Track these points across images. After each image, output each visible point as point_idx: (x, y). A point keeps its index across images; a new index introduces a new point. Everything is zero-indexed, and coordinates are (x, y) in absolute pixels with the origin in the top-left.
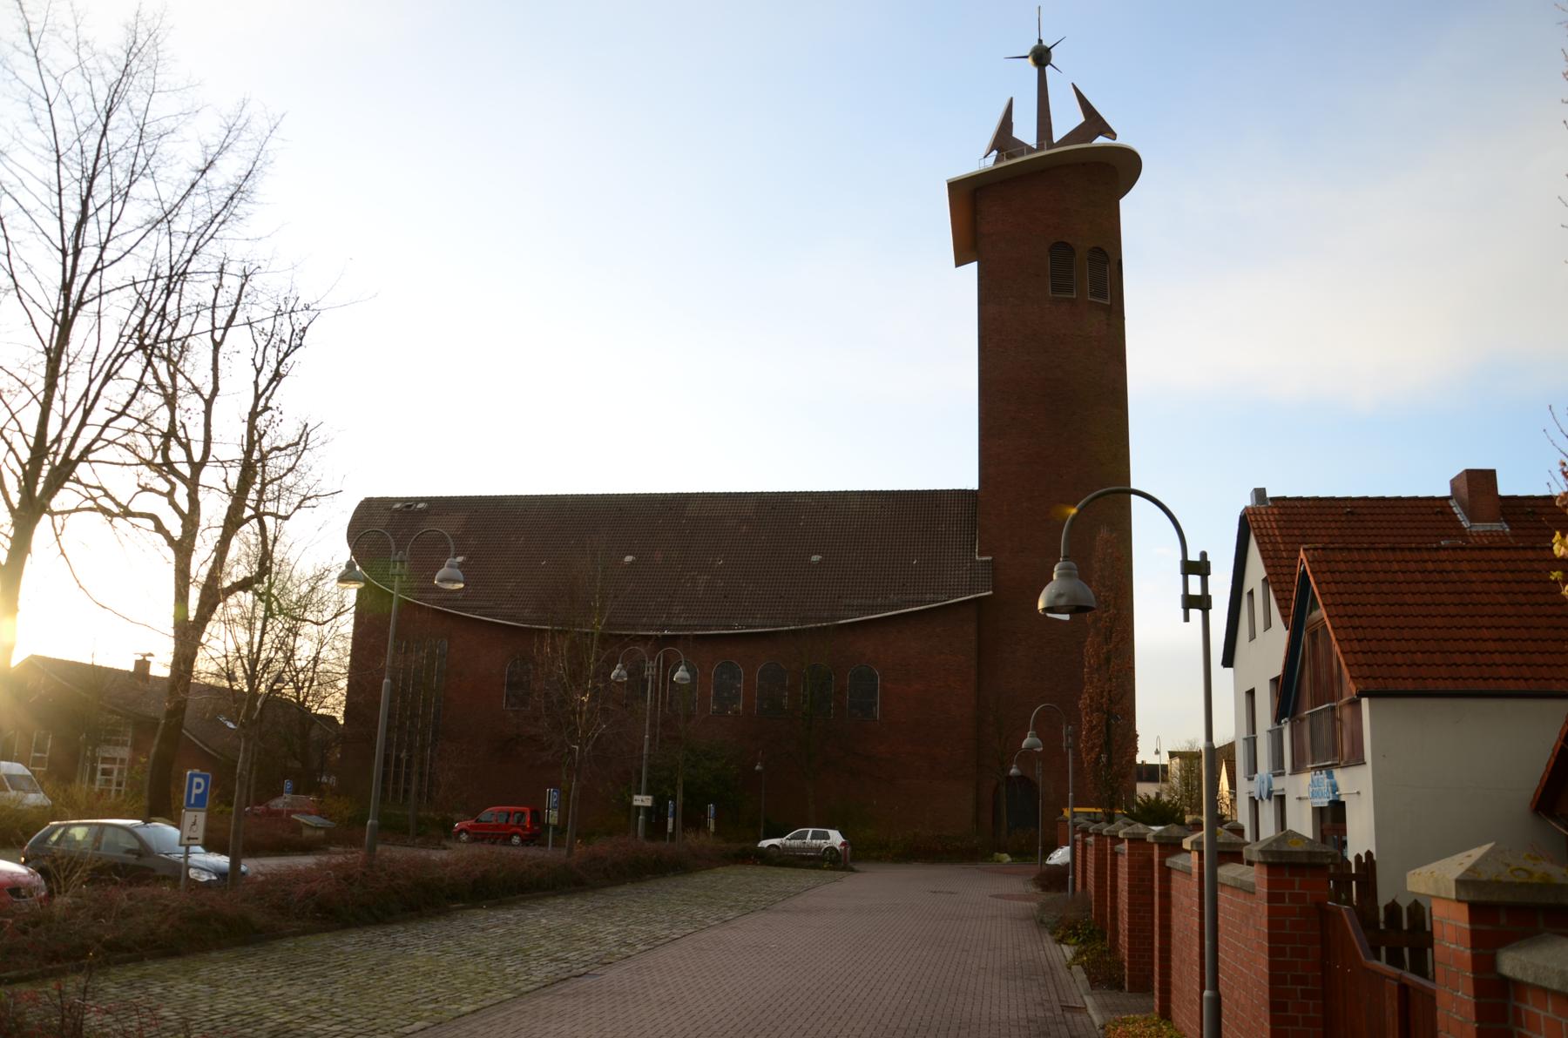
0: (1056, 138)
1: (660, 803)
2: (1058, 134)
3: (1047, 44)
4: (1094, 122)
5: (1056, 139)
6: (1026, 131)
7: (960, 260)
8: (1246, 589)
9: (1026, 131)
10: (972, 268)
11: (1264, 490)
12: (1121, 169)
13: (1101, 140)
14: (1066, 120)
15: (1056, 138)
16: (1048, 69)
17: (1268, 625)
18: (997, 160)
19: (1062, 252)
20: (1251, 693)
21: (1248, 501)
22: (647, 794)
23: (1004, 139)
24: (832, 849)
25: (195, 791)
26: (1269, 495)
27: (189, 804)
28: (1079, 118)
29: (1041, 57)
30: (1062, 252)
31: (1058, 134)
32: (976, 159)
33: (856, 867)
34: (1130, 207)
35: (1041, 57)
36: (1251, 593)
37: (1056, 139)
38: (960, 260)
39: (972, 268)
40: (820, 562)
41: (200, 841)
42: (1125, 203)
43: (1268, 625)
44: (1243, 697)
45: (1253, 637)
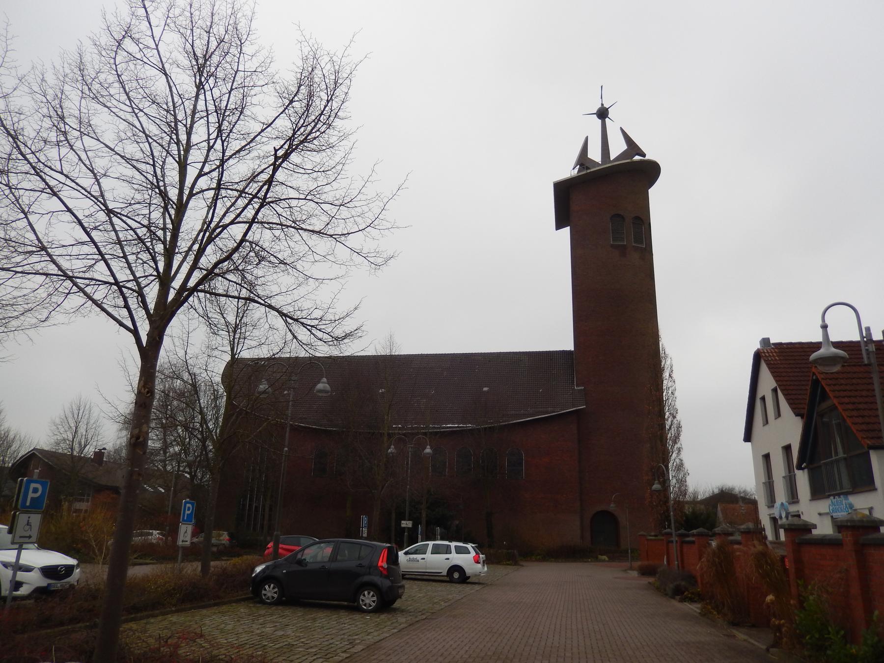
0: (612, 157)
1: (415, 526)
2: (613, 155)
3: (606, 106)
4: (633, 147)
5: (612, 159)
6: (595, 154)
7: (559, 225)
8: (759, 395)
9: (595, 154)
10: (567, 231)
11: (768, 339)
12: (649, 172)
13: (637, 158)
14: (617, 147)
15: (612, 157)
16: (607, 119)
17: (778, 414)
18: (579, 171)
19: (618, 218)
20: (767, 457)
21: (757, 346)
22: (409, 520)
23: (583, 160)
24: (152, 545)
25: (187, 512)
26: (772, 341)
27: (183, 520)
28: (624, 147)
29: (603, 114)
30: (618, 218)
31: (613, 155)
32: (568, 170)
33: (522, 563)
34: (655, 193)
35: (603, 114)
36: (763, 399)
37: (612, 159)
38: (559, 225)
39: (567, 231)
40: (488, 392)
41: (34, 539)
42: (652, 192)
43: (778, 414)
44: (761, 460)
45: (766, 422)
